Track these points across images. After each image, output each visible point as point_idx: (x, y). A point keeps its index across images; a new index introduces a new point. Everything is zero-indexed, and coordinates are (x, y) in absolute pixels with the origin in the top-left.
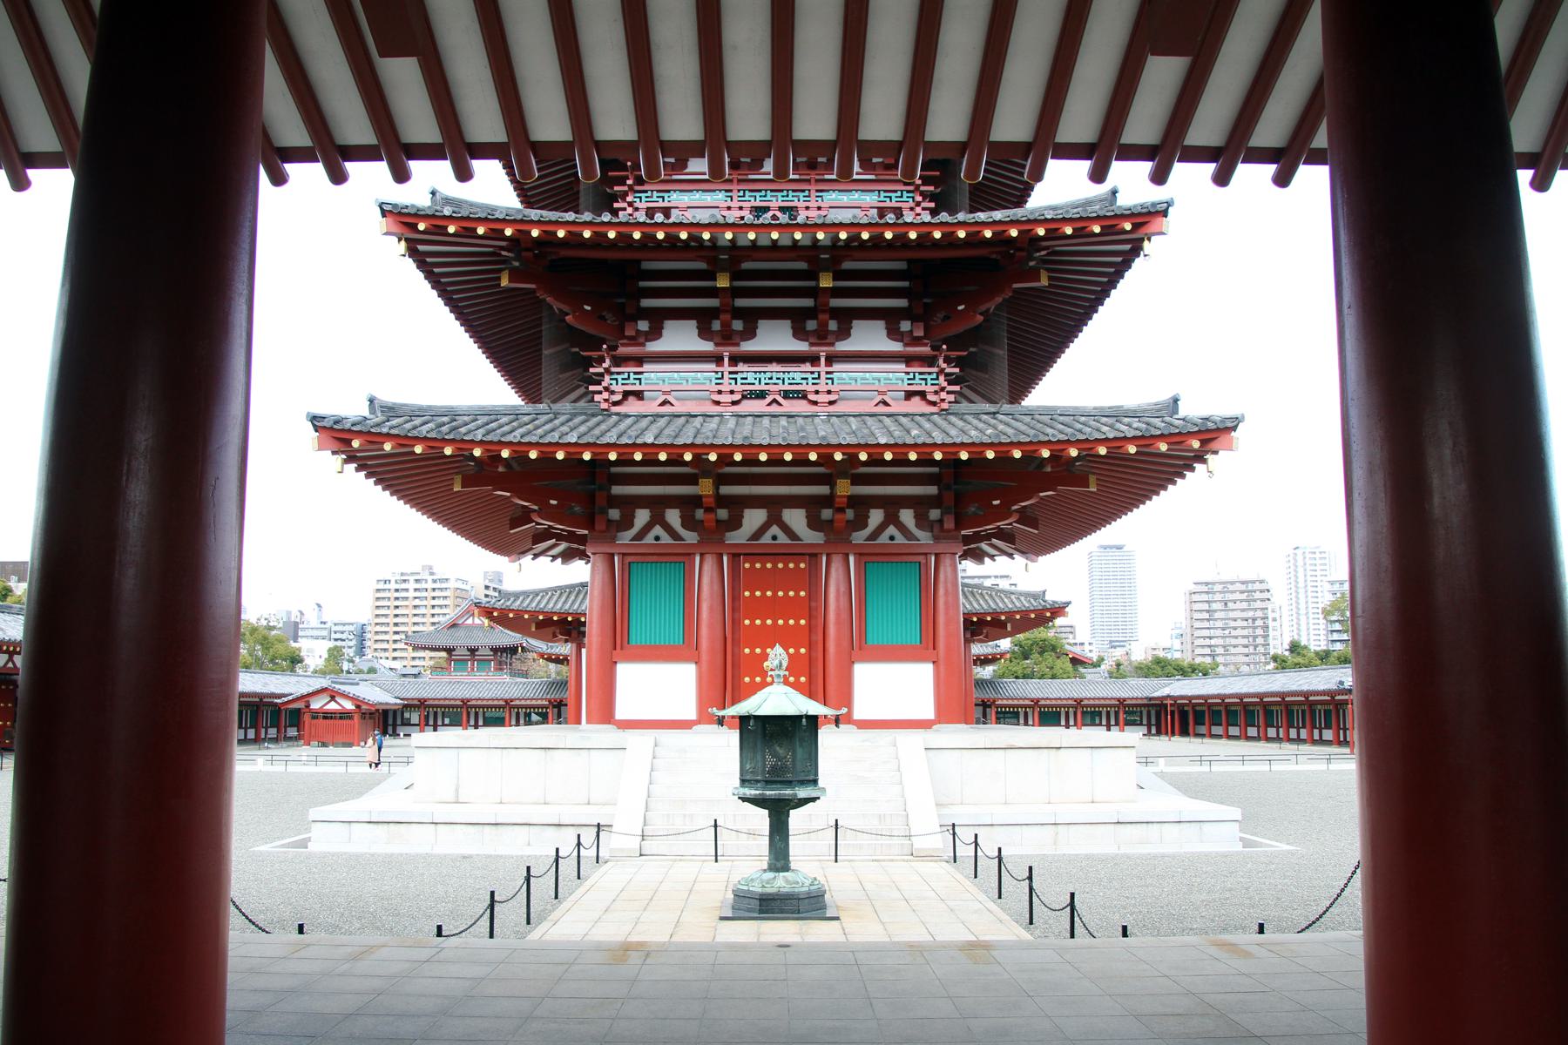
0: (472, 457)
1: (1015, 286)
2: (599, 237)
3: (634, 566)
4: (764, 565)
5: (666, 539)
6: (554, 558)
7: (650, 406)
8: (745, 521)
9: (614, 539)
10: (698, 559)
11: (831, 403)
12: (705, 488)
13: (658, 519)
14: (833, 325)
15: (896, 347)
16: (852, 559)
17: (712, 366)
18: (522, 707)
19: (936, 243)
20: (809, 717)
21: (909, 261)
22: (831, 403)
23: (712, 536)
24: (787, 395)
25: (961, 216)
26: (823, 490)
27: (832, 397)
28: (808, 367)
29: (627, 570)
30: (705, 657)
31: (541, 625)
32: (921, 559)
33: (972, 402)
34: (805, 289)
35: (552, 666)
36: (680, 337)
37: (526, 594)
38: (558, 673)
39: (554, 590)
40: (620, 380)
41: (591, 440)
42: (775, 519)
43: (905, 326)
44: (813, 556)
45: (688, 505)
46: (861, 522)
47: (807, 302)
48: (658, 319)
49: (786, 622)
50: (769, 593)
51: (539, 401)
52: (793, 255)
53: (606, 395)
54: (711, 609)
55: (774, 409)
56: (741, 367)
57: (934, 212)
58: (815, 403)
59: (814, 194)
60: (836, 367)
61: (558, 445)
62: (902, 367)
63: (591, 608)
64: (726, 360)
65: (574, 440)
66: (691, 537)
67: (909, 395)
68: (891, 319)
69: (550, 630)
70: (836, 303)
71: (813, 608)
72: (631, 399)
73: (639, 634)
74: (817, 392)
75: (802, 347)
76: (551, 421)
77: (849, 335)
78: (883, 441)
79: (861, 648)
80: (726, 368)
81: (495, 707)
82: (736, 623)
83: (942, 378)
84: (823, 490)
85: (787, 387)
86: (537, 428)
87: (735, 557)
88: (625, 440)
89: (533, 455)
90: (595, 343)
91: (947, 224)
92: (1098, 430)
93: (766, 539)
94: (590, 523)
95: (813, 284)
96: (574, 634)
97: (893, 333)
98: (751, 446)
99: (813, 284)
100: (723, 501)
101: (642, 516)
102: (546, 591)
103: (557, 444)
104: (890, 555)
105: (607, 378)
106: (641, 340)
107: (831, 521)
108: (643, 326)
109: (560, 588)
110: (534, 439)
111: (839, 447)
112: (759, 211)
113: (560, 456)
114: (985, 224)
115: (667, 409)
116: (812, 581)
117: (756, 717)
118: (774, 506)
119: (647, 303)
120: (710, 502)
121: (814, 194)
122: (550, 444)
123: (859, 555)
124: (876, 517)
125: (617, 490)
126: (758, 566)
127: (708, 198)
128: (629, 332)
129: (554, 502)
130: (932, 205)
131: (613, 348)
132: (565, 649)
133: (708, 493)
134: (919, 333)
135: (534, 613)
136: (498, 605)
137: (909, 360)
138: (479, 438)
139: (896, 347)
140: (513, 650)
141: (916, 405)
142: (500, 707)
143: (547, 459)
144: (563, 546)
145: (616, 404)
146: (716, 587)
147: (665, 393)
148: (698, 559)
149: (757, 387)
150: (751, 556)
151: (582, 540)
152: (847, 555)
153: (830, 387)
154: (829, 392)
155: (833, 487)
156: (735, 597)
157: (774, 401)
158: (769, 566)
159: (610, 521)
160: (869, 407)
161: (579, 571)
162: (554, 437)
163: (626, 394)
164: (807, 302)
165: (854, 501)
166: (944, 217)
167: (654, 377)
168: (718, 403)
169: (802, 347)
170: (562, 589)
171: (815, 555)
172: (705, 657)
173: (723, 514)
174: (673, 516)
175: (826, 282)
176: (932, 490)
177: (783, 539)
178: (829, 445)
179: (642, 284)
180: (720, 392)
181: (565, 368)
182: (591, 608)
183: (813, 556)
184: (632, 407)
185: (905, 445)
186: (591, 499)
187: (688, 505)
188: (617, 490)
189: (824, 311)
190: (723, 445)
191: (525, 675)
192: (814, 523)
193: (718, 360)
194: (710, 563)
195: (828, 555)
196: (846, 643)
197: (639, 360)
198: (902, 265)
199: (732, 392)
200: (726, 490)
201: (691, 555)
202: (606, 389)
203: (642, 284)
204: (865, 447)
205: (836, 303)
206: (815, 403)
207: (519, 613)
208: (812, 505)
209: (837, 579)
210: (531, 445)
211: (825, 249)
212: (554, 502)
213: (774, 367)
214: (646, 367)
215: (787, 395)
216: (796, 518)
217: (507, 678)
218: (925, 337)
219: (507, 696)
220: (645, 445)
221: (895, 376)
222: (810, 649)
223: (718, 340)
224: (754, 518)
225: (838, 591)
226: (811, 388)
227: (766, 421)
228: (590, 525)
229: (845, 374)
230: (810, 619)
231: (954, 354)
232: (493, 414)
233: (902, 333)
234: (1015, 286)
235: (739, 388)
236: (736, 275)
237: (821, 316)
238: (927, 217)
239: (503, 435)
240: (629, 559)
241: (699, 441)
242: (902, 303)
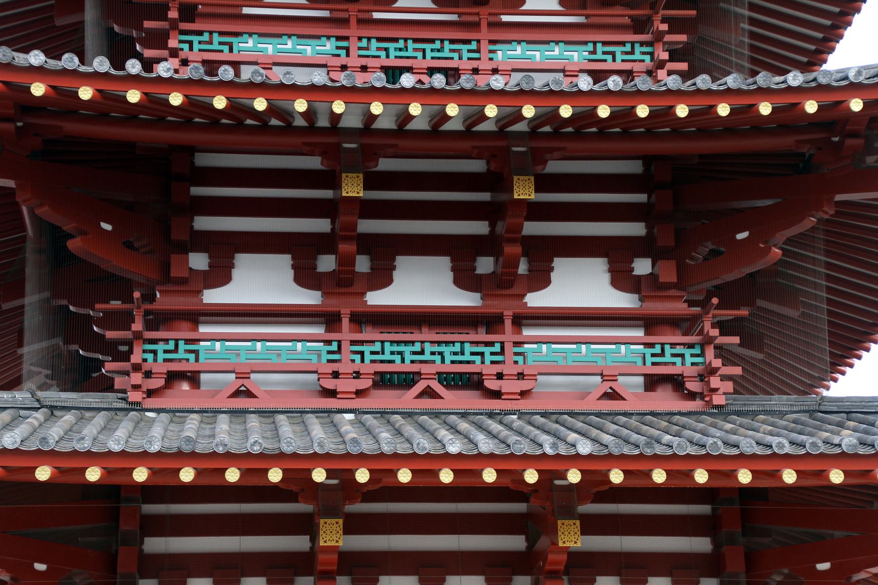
1: (839, 197)
2: (703, 116)
14: (363, 264)
19: (760, 125)
21: (648, 160)
25: (732, 81)
26: (298, 543)
33: (756, 394)
34: (497, 197)
36: (263, 281)
40: (158, 354)
43: (642, 267)
47: (321, 225)
48: (225, 251)
52: (466, 145)
57: (685, 76)
58: (497, 395)
59: (485, 46)
68: (617, 255)
70: (368, 226)
74: (500, 376)
75: (467, 300)
83: (710, 352)
84: (298, 543)
85: (448, 368)
90: (121, 287)
91: (739, 92)
92: (627, 441)
95: (327, 194)
97: (622, 279)
99: (327, 194)
108: (199, 261)
112: (393, 73)
114: (765, 93)
119: (205, 223)
121: (485, 46)
125: (155, 545)
127: (309, 50)
129: (40, 567)
130: (683, 66)
134: (668, 274)
137: (651, 324)
141: (665, 400)
145: (150, 393)
149: (398, 367)
155: (314, 539)
163: (173, 377)
164: (321, 225)
166: (703, 81)
169: (467, 300)
175: (352, 188)
176: (701, 544)
179: (197, 191)
180: (336, 375)
189: (347, 239)
198: (633, 167)
199: (357, 375)
203: (197, 191)
205: (368, 226)
206: (497, 395)
211: (350, 133)
212: (40, 567)
213: (427, 334)
218: (678, 286)
221: (625, 352)
229: (540, 348)
231: (728, 314)
234: (839, 197)
236: (373, 181)
237: (345, 247)
238: (673, 82)
242: (635, 229)
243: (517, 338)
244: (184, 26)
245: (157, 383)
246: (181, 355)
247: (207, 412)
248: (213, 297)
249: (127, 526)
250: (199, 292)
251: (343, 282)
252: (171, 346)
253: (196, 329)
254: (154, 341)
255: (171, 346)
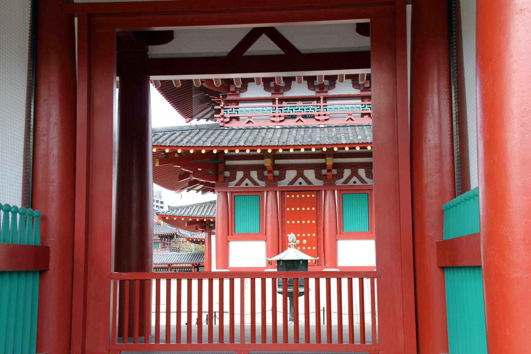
0: (164, 152)
3: (236, 198)
4: (295, 196)
5: (251, 185)
6: (198, 191)
7: (242, 124)
8: (287, 176)
9: (227, 186)
10: (265, 193)
11: (326, 120)
12: (267, 162)
13: (247, 176)
15: (357, 92)
16: (336, 192)
17: (271, 104)
18: (178, 268)
20: (303, 261)
22: (326, 120)
23: (272, 183)
24: (304, 117)
27: (326, 117)
28: (315, 103)
29: (233, 199)
30: (269, 238)
31: (190, 223)
32: (369, 192)
35: (193, 245)
37: (182, 208)
38: (196, 249)
39: (197, 205)
40: (229, 112)
41: (217, 145)
42: (300, 175)
44: (318, 192)
45: (260, 169)
46: (340, 176)
49: (306, 222)
50: (303, 209)
51: (192, 117)
53: (222, 119)
54: (272, 216)
55: (300, 123)
56: (284, 104)
58: (319, 120)
60: (329, 102)
61: (202, 147)
62: (360, 101)
63: (216, 214)
64: (277, 101)
65: (209, 145)
66: (262, 184)
67: (363, 115)
69: (195, 226)
71: (318, 215)
72: (234, 120)
73: (239, 229)
74: (319, 115)
76: (198, 133)
77: (335, 87)
78: (344, 142)
79: (340, 233)
80: (277, 105)
81: (163, 268)
82: (283, 223)
85: (305, 113)
86: (192, 138)
87: (282, 193)
88: (231, 144)
89: (192, 151)
93: (296, 184)
94: (216, 178)
96: (207, 227)
98: (286, 146)
100: (276, 167)
101: (240, 175)
102: (192, 206)
103: (202, 147)
104: (355, 190)
105: (222, 111)
106: (238, 92)
107: (326, 175)
109: (199, 204)
110: (192, 145)
111: (325, 145)
113: (203, 152)
115: (250, 125)
116: (318, 203)
117: (283, 261)
118: (300, 168)
120: (271, 168)
122: (199, 147)
123: (339, 191)
124: (347, 173)
125: (228, 163)
126: (298, 196)
128: (232, 89)
129: (200, 169)
131: (224, 96)
132: (202, 235)
133: (271, 165)
135: (186, 218)
136: (168, 214)
138: (168, 144)
139: (357, 92)
140: (171, 237)
142: (165, 268)
143: (198, 153)
144: (201, 186)
145: (227, 123)
146: (274, 206)
147: (249, 117)
148: (265, 193)
150: (290, 192)
151: (213, 185)
152: (334, 191)
153: (325, 113)
154: (325, 115)
156: (283, 211)
157: (300, 120)
158: (298, 196)
159: (225, 177)
160: (343, 122)
161: (211, 196)
162: (200, 143)
163: (231, 118)
165: (335, 166)
167: (244, 109)
168: (273, 121)
170: (200, 205)
171: (319, 191)
172: (269, 238)
173: (277, 173)
174: (254, 174)
177: (304, 184)
178: (320, 145)
180: (274, 116)
181: (202, 102)
182: (216, 214)
183: (318, 192)
184: (234, 124)
185: (354, 144)
186: (216, 167)
187: (260, 169)
188: (228, 163)
190: (274, 146)
191: (178, 250)
192: (318, 176)
193: (273, 101)
194: (271, 194)
195: (325, 191)
196: (334, 231)
197: (237, 102)
199: (280, 116)
200: (277, 162)
201: (262, 192)
202: (222, 116)
204: (336, 145)
206: (319, 120)
207: (179, 217)
208: (318, 168)
209: (329, 201)
210: (190, 147)
212: (200, 169)
213: (300, 104)
214: (241, 105)
215: (304, 117)
216: (310, 174)
217: (169, 253)
219: (169, 262)
220: (240, 146)
222: (317, 235)
223: (273, 92)
224: (291, 174)
225: (330, 207)
226: (316, 113)
227: (294, 131)
228: (216, 179)
230: (317, 221)
232: (172, 131)
233: (360, 85)
235: (283, 114)
239: (178, 143)
240: (234, 194)
241: (263, 144)
243: (325, 104)
244: (225, 107)
245: (228, 120)
246: (234, 112)
247: (31, 324)
248: (243, 95)
249: (221, 168)
250: (238, 95)
251: (277, 90)
252: (231, 110)
253: (238, 105)
254: (226, 109)
255: (231, 110)
